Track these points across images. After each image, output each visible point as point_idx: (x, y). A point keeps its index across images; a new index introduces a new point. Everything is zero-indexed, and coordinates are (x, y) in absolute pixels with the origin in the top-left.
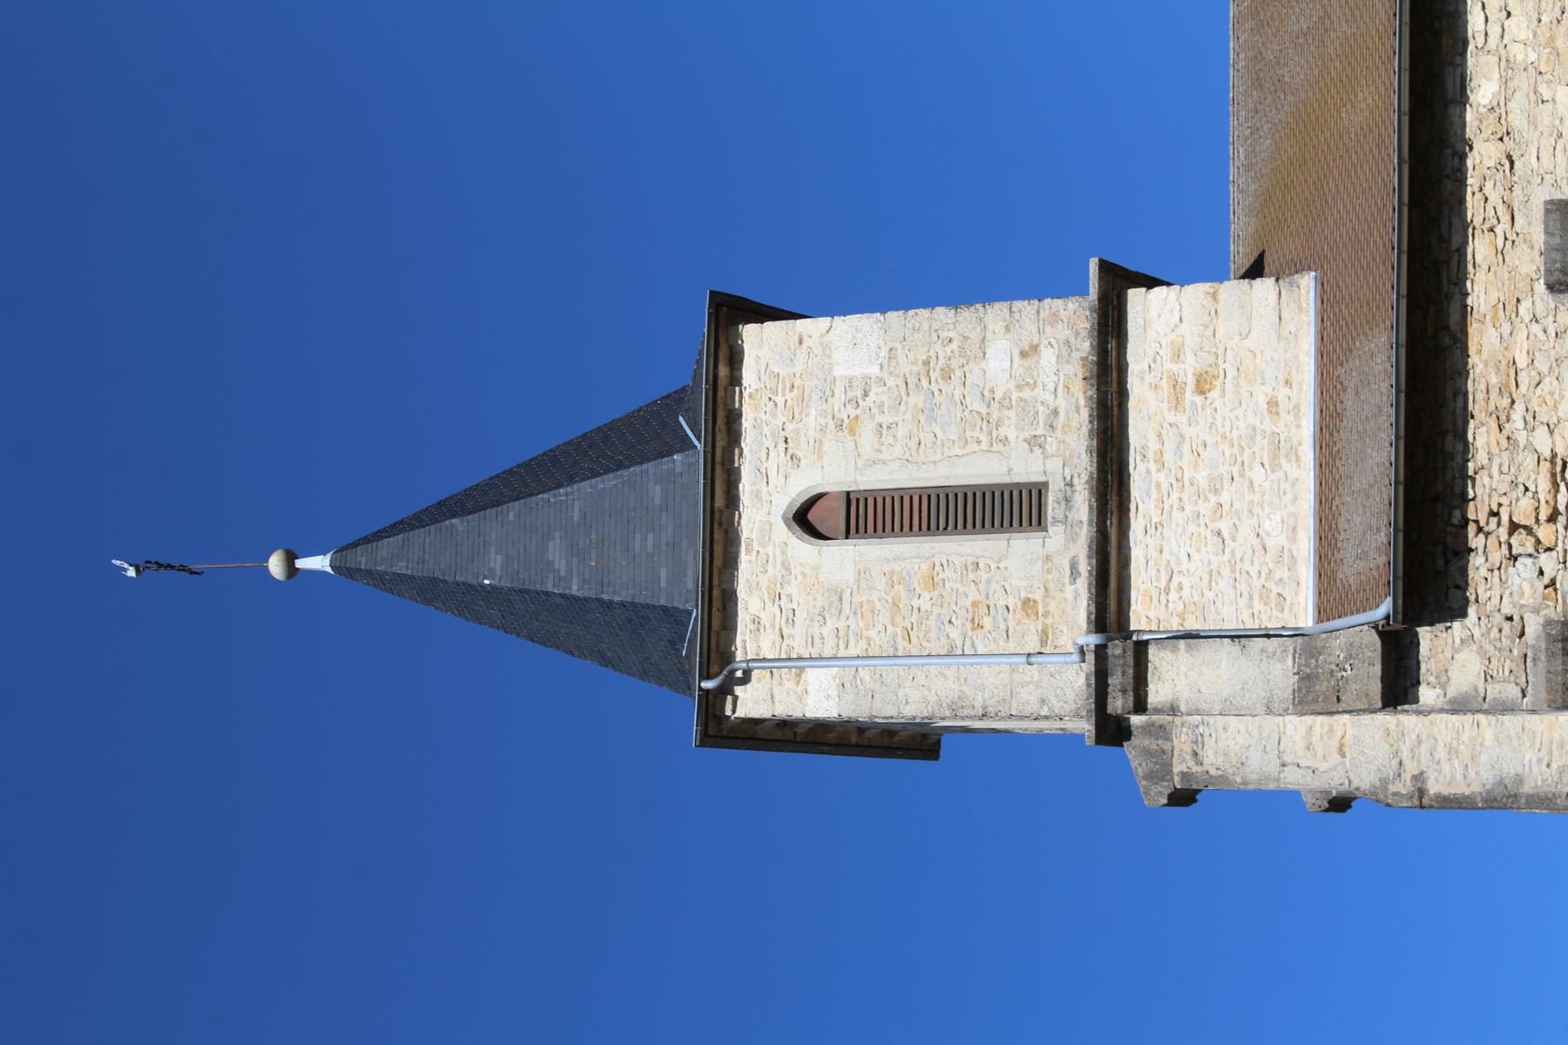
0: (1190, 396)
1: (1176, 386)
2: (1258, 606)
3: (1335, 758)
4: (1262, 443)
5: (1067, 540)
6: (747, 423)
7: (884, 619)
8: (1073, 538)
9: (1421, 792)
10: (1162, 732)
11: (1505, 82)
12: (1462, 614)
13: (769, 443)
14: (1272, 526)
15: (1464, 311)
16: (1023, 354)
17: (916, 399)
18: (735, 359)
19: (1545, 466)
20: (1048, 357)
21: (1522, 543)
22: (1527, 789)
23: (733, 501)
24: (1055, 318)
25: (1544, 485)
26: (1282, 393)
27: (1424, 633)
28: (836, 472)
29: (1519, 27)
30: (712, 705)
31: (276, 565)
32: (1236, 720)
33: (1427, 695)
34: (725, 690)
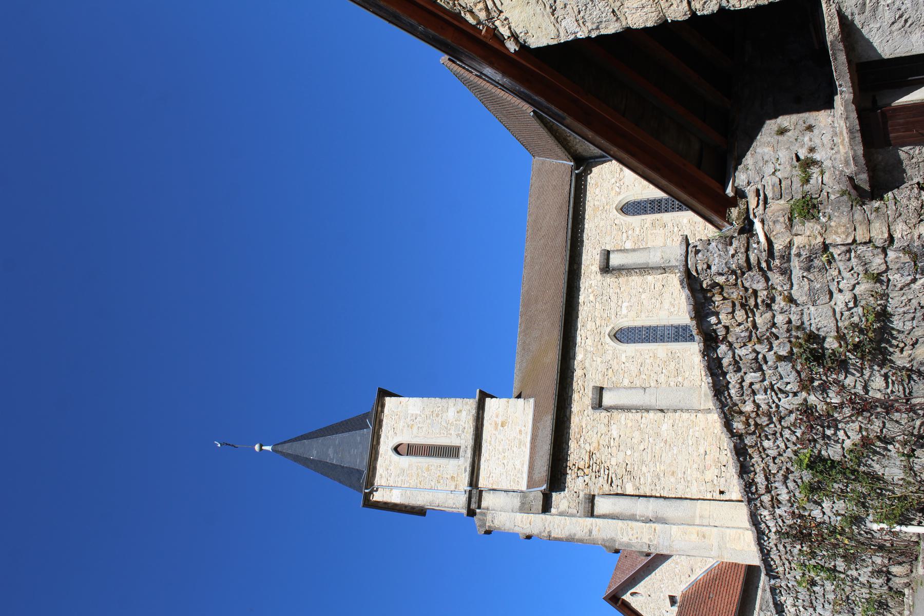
1: (496, 424)
6: (384, 423)
10: (484, 514)
11: (585, 355)
14: (518, 463)
17: (429, 421)
18: (383, 406)
20: (464, 413)
21: (580, 473)
23: (378, 443)
25: (587, 459)
26: (523, 429)
27: (554, 494)
28: (406, 438)
29: (589, 342)
30: (367, 496)
31: (257, 447)
32: (505, 513)
33: (553, 510)
34: (371, 493)
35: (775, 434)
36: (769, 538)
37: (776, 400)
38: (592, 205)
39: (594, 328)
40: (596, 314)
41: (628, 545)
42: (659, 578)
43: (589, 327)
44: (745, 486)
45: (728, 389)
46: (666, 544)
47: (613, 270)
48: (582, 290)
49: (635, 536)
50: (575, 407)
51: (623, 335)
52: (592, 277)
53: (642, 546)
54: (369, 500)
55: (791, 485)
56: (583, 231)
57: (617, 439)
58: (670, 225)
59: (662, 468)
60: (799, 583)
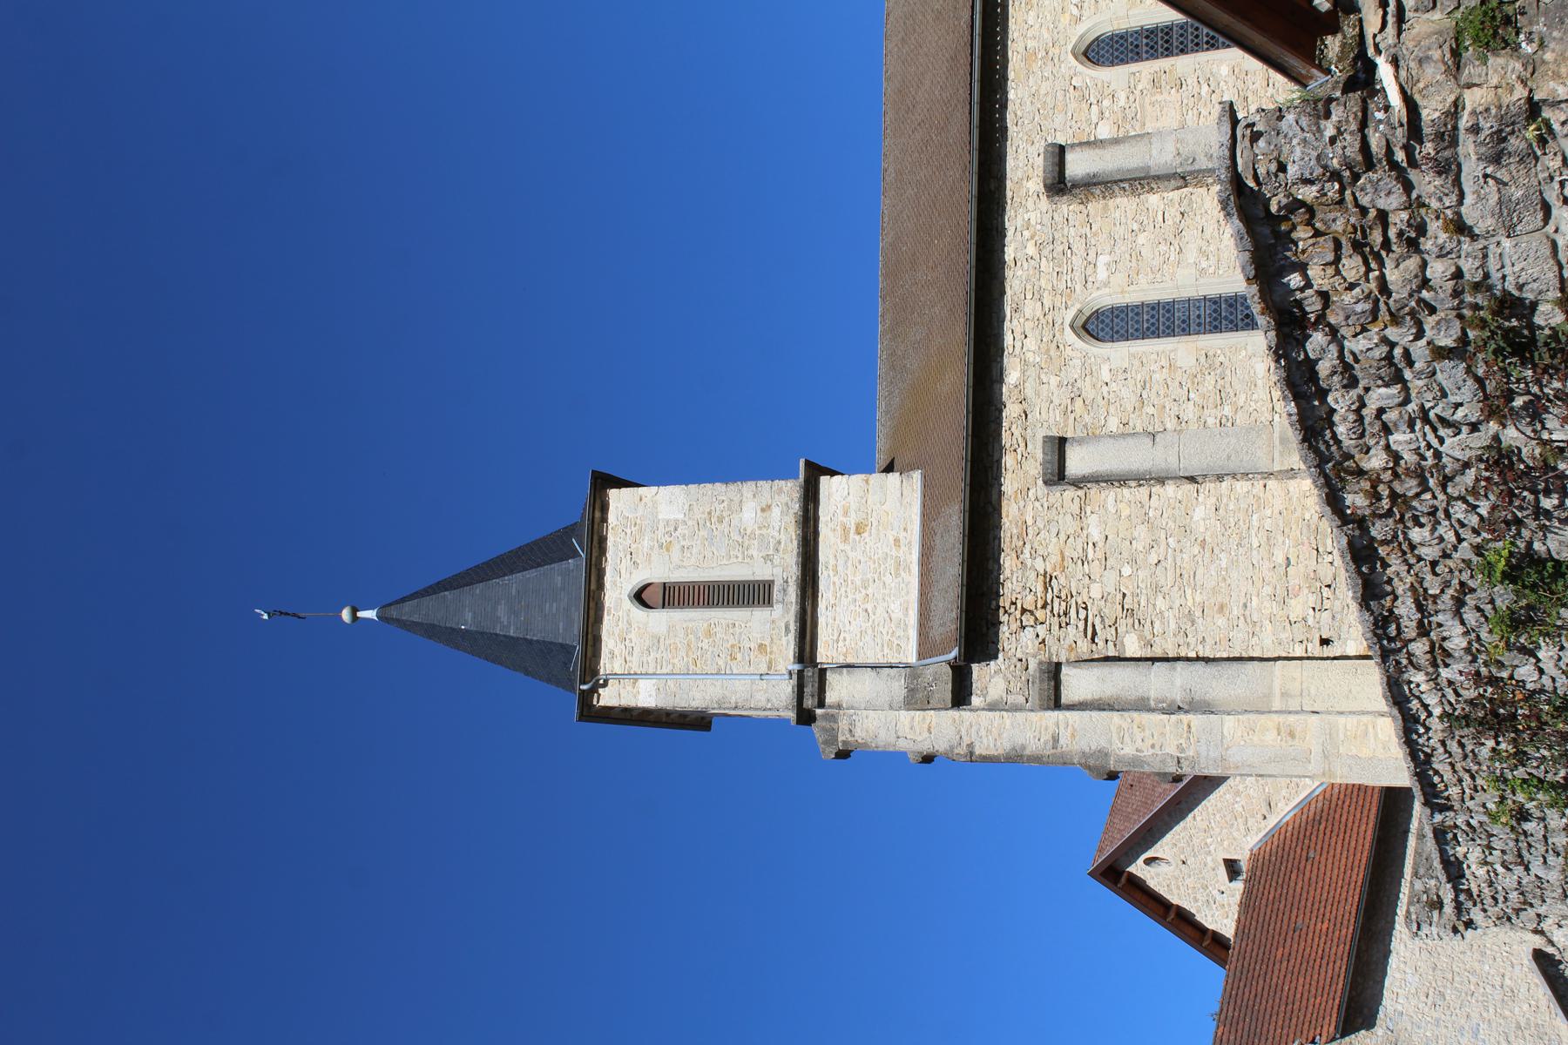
1: (845, 530)
2: (886, 651)
4: (890, 562)
5: (784, 612)
6: (610, 543)
8: (787, 612)
9: (972, 753)
11: (1023, 372)
12: (996, 658)
13: (621, 554)
15: (1000, 494)
16: (763, 510)
17: (703, 533)
18: (604, 508)
20: (776, 512)
22: (1028, 752)
24: (780, 491)
25: (1040, 589)
26: (902, 535)
27: (975, 667)
28: (658, 572)
29: (1031, 343)
30: (586, 699)
31: (346, 615)
32: (876, 713)
33: (976, 700)
34: (594, 690)
35: (1433, 513)
36: (1428, 729)
37: (1435, 443)
38: (1021, 49)
39: (1039, 313)
40: (1043, 283)
41: (1136, 761)
43: (1028, 311)
45: (1331, 425)
47: (1074, 186)
48: (1010, 234)
50: (1009, 484)
51: (1104, 325)
52: (1030, 205)
55: (1471, 617)
56: (1004, 106)
57: (1100, 544)
58: (1192, 81)
59: (1198, 599)
60: (1494, 818)
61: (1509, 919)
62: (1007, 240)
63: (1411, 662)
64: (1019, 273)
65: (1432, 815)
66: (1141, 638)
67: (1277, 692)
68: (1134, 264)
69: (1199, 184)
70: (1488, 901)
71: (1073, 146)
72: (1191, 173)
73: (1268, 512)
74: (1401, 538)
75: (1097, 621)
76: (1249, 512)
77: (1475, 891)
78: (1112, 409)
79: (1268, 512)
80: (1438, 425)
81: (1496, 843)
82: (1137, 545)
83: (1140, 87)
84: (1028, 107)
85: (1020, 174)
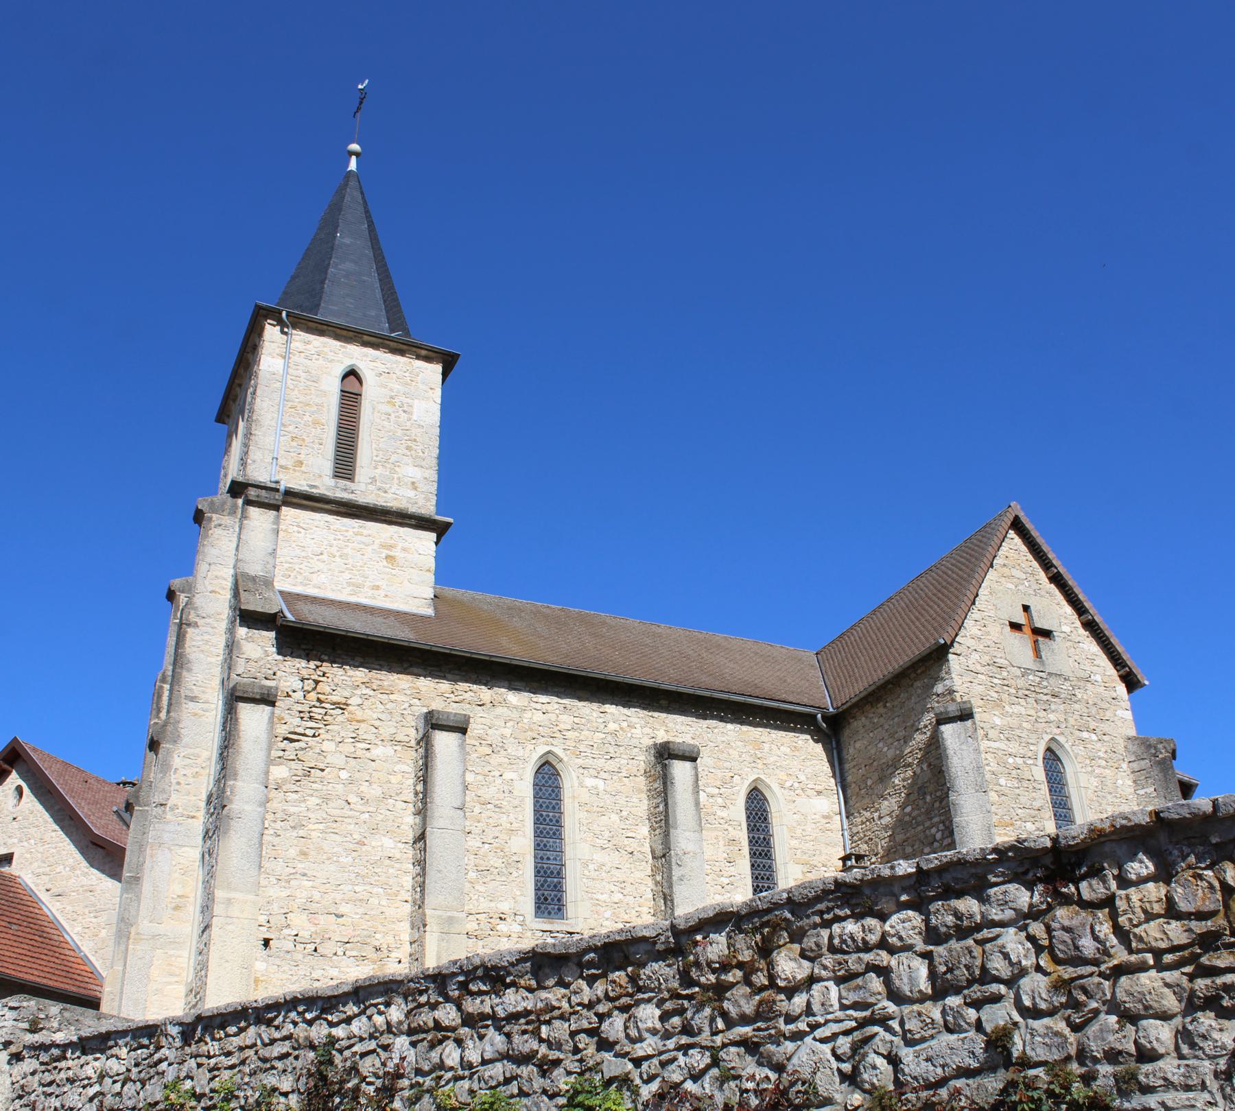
0: (385, 552)
1: (391, 547)
2: (287, 565)
3: (210, 588)
4: (360, 580)
5: (327, 485)
6: (399, 358)
7: (302, 398)
8: (328, 489)
9: (189, 625)
10: (233, 512)
11: (516, 707)
13: (388, 365)
14: (323, 578)
15: (418, 675)
16: (413, 483)
17: (399, 433)
18: (428, 359)
19: (344, 701)
20: (411, 494)
21: (309, 685)
22: (185, 673)
23: (365, 344)
24: (428, 500)
25: (335, 699)
26: (382, 593)
27: (273, 634)
28: (371, 392)
29: (538, 717)
30: (274, 314)
31: (355, 147)
32: (233, 550)
33: (242, 632)
34: (280, 322)
35: (687, 1030)
36: (310, 1023)
37: (819, 1033)
38: (763, 738)
39: (562, 726)
40: (585, 733)
41: (166, 768)
42: (47, 838)
43: (564, 718)
44: (494, 968)
45: (857, 917)
46: (166, 836)
47: (665, 767)
48: (625, 711)
49: (182, 780)
50: (426, 684)
51: (547, 779)
52: (647, 730)
53: (163, 791)
54: (266, 317)
55: (498, 1071)
56: (722, 720)
57: (368, 755)
58: (732, 870)
59: (313, 834)
60: (174, 1086)
61: (20, 1097)
62: (620, 708)
63: (420, 1006)
64: (595, 714)
65: (181, 1024)
66: (284, 780)
67: (232, 895)
68: (595, 809)
69: (655, 870)
70: (48, 1077)
71: (696, 768)
72: (669, 863)
73: (384, 902)
74: (640, 996)
75: (302, 744)
76: (385, 886)
77: (63, 1064)
78: (480, 777)
79: (384, 902)
80: (857, 1035)
81: (130, 1089)
82: (364, 787)
83: (730, 829)
84: (720, 739)
85: (671, 725)
